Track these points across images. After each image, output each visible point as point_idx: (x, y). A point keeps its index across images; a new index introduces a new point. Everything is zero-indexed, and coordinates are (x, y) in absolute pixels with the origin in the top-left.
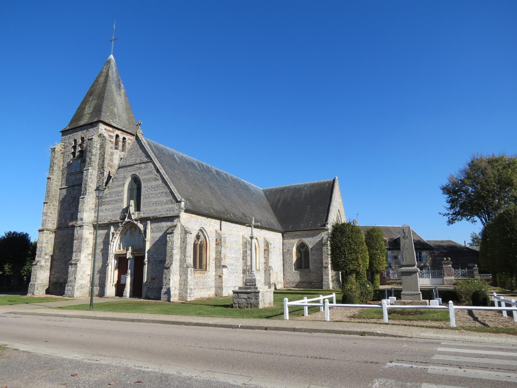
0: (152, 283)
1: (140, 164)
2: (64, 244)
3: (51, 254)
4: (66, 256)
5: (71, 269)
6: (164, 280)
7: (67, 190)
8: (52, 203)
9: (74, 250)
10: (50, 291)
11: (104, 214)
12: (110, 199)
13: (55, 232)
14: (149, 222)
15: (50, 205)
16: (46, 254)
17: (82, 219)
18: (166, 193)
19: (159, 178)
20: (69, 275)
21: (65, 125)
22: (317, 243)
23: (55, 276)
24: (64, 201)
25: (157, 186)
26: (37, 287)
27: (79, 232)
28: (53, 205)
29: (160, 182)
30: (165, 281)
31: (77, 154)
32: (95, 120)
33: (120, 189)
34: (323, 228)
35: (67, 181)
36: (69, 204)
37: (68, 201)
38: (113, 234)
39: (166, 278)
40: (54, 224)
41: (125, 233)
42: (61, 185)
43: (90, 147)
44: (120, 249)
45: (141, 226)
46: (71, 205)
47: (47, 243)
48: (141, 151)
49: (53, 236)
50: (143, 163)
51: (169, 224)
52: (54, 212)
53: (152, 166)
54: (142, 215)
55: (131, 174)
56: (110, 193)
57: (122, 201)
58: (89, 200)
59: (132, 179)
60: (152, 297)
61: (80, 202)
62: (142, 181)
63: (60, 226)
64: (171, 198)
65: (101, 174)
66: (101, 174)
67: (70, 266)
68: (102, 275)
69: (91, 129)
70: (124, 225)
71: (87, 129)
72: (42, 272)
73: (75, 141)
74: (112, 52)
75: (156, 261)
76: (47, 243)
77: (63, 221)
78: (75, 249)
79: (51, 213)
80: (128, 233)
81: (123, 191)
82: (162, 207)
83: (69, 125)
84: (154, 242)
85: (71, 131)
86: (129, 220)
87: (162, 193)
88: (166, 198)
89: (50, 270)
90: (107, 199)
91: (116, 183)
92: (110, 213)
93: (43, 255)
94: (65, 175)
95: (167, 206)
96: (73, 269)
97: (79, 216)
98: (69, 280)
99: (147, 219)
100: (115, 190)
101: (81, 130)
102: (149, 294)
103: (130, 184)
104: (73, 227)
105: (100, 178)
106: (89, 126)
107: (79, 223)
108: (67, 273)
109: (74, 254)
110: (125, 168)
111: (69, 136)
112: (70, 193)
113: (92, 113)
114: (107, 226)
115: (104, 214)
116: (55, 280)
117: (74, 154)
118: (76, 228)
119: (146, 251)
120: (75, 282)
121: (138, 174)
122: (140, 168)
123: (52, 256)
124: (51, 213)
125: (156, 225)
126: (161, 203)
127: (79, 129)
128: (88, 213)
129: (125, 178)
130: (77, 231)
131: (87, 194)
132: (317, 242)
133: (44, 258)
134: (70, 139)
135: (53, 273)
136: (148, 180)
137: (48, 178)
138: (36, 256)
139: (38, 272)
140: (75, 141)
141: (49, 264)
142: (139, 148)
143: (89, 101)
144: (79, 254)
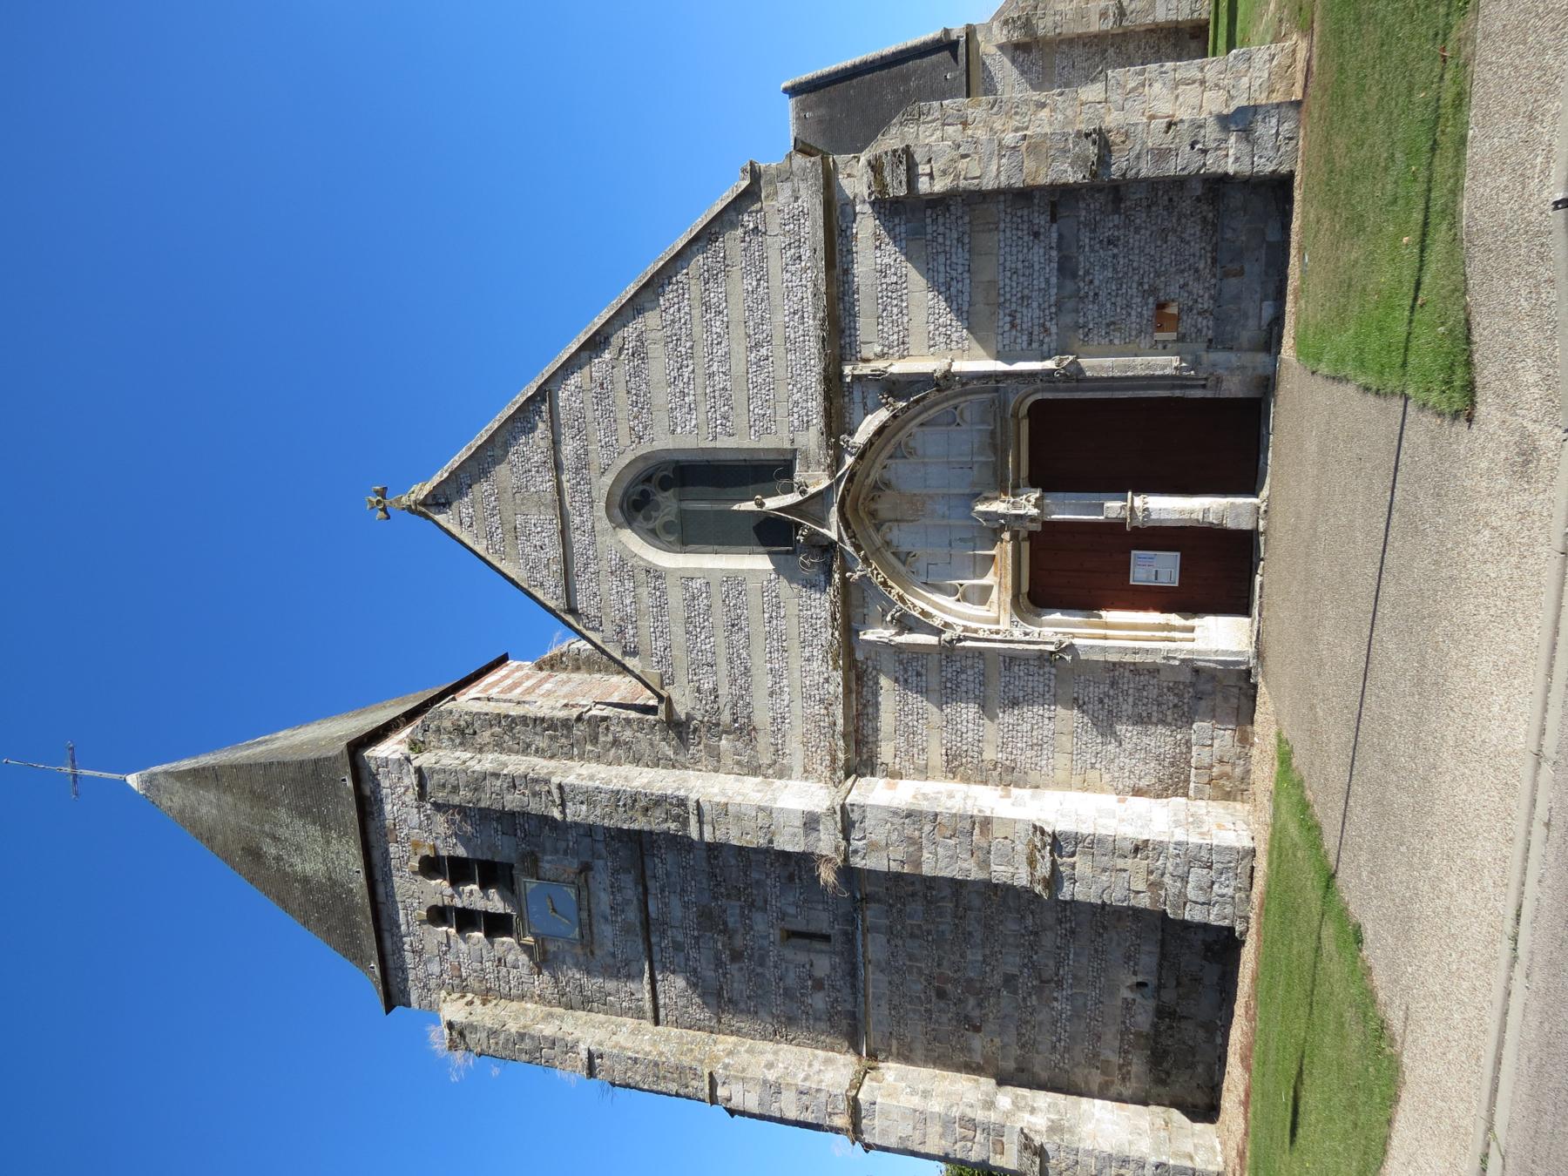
0: (1187, 323)
1: (558, 467)
2: (941, 994)
3: (987, 1084)
4: (1009, 980)
5: (1087, 884)
6: (1173, 168)
7: (664, 969)
8: (717, 1059)
9: (976, 874)
10: (1201, 1099)
11: (797, 707)
12: (723, 666)
13: (872, 1055)
14: (847, 370)
15: (726, 1067)
16: (990, 1105)
17: (811, 822)
18: (710, 277)
19: (630, 331)
20: (1116, 897)
21: (366, 984)
22: (1023, 73)
23: (1116, 1059)
24: (720, 995)
25: (673, 340)
26: (1176, 1155)
27: (878, 836)
28: (730, 1053)
29: (651, 319)
30: (1181, 163)
31: (495, 903)
32: (349, 783)
33: (675, 597)
34: (962, 50)
35: (621, 970)
36: (736, 956)
37: (719, 964)
38: (906, 623)
39: (1161, 154)
40: (827, 1061)
41: (903, 557)
42: (639, 1014)
43: (455, 789)
44: (983, 595)
45: (868, 426)
46: (738, 942)
47: (926, 1094)
48: (502, 470)
49: (891, 1071)
50: (556, 444)
51: (866, 226)
52: (770, 1057)
53: (575, 379)
54: (811, 439)
55: (605, 524)
56: (694, 667)
57: (734, 580)
58: (716, 790)
59: (629, 523)
60: (1268, 311)
61: (720, 836)
62: (644, 449)
63: (845, 1024)
64: (732, 241)
65: (594, 740)
66: (594, 740)
67: (1066, 893)
68: (1127, 708)
69: (388, 808)
70: (858, 548)
71: (386, 834)
72: (1086, 1129)
73: (438, 915)
74: (116, 776)
75: (1059, 305)
76: (926, 1094)
77: (819, 1001)
78: (966, 868)
79: (770, 1066)
80: (902, 536)
81: (687, 578)
82: (776, 298)
83: (359, 959)
84: (959, 332)
85: (388, 944)
86: (834, 516)
87: (707, 306)
88: (736, 273)
89: (1081, 1095)
90: (723, 690)
91: (646, 624)
92: (796, 664)
93: (993, 1117)
94: (593, 984)
95: (775, 264)
96: (1082, 865)
97: (789, 842)
98: (1144, 901)
99: (834, 386)
100: (678, 631)
101: (388, 876)
102: (1249, 332)
103: (653, 536)
104: (848, 873)
105: (616, 742)
106: (372, 826)
107: (826, 842)
108: (1104, 917)
109: (1001, 872)
110: (578, 565)
111: (408, 956)
112: (678, 947)
113: (325, 827)
114: (858, 671)
115: (797, 707)
116: (1138, 1066)
117: (496, 925)
118: (857, 862)
119: (1001, 366)
120: (1160, 848)
121: (608, 480)
122: (583, 464)
123: (1001, 1082)
124: (770, 1066)
125: (865, 327)
126: (759, 302)
127: (381, 889)
128: (776, 798)
129: (624, 567)
130: (873, 847)
131: (682, 793)
132: (1015, 73)
133: (1007, 1114)
134: (428, 949)
135: (1096, 1078)
136: (641, 404)
137: (591, 1070)
138: (996, 1161)
139: (1087, 1145)
140: (438, 915)
141: (1043, 1099)
142: (484, 486)
143: (278, 858)
144: (998, 831)
